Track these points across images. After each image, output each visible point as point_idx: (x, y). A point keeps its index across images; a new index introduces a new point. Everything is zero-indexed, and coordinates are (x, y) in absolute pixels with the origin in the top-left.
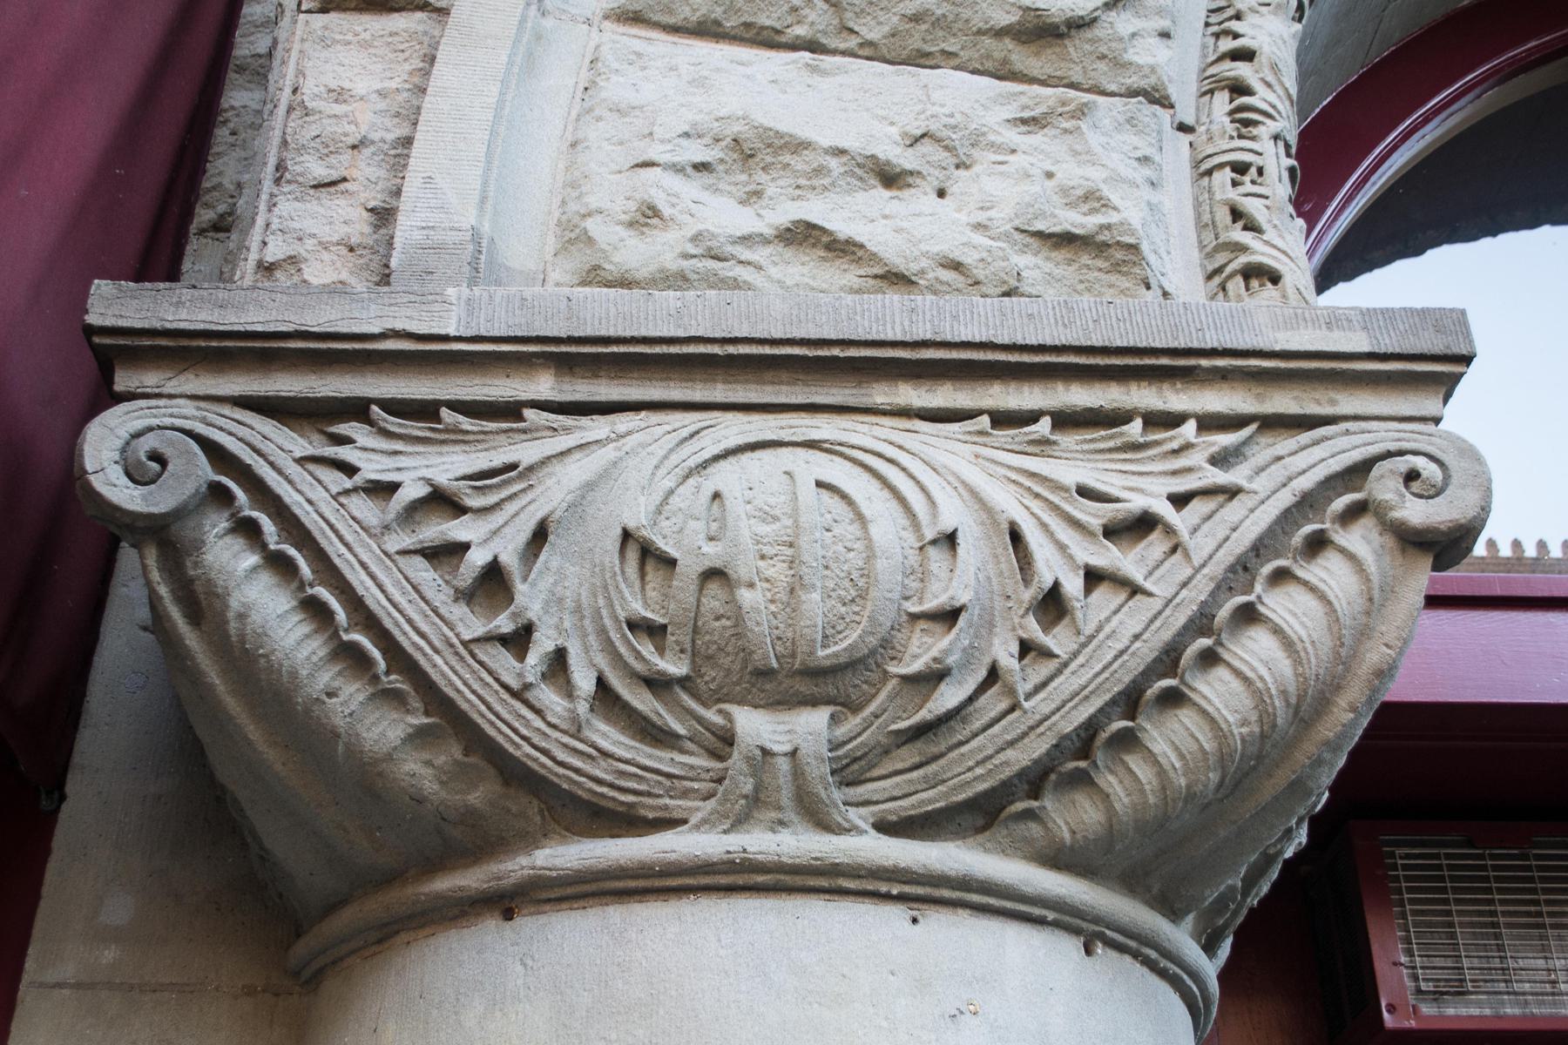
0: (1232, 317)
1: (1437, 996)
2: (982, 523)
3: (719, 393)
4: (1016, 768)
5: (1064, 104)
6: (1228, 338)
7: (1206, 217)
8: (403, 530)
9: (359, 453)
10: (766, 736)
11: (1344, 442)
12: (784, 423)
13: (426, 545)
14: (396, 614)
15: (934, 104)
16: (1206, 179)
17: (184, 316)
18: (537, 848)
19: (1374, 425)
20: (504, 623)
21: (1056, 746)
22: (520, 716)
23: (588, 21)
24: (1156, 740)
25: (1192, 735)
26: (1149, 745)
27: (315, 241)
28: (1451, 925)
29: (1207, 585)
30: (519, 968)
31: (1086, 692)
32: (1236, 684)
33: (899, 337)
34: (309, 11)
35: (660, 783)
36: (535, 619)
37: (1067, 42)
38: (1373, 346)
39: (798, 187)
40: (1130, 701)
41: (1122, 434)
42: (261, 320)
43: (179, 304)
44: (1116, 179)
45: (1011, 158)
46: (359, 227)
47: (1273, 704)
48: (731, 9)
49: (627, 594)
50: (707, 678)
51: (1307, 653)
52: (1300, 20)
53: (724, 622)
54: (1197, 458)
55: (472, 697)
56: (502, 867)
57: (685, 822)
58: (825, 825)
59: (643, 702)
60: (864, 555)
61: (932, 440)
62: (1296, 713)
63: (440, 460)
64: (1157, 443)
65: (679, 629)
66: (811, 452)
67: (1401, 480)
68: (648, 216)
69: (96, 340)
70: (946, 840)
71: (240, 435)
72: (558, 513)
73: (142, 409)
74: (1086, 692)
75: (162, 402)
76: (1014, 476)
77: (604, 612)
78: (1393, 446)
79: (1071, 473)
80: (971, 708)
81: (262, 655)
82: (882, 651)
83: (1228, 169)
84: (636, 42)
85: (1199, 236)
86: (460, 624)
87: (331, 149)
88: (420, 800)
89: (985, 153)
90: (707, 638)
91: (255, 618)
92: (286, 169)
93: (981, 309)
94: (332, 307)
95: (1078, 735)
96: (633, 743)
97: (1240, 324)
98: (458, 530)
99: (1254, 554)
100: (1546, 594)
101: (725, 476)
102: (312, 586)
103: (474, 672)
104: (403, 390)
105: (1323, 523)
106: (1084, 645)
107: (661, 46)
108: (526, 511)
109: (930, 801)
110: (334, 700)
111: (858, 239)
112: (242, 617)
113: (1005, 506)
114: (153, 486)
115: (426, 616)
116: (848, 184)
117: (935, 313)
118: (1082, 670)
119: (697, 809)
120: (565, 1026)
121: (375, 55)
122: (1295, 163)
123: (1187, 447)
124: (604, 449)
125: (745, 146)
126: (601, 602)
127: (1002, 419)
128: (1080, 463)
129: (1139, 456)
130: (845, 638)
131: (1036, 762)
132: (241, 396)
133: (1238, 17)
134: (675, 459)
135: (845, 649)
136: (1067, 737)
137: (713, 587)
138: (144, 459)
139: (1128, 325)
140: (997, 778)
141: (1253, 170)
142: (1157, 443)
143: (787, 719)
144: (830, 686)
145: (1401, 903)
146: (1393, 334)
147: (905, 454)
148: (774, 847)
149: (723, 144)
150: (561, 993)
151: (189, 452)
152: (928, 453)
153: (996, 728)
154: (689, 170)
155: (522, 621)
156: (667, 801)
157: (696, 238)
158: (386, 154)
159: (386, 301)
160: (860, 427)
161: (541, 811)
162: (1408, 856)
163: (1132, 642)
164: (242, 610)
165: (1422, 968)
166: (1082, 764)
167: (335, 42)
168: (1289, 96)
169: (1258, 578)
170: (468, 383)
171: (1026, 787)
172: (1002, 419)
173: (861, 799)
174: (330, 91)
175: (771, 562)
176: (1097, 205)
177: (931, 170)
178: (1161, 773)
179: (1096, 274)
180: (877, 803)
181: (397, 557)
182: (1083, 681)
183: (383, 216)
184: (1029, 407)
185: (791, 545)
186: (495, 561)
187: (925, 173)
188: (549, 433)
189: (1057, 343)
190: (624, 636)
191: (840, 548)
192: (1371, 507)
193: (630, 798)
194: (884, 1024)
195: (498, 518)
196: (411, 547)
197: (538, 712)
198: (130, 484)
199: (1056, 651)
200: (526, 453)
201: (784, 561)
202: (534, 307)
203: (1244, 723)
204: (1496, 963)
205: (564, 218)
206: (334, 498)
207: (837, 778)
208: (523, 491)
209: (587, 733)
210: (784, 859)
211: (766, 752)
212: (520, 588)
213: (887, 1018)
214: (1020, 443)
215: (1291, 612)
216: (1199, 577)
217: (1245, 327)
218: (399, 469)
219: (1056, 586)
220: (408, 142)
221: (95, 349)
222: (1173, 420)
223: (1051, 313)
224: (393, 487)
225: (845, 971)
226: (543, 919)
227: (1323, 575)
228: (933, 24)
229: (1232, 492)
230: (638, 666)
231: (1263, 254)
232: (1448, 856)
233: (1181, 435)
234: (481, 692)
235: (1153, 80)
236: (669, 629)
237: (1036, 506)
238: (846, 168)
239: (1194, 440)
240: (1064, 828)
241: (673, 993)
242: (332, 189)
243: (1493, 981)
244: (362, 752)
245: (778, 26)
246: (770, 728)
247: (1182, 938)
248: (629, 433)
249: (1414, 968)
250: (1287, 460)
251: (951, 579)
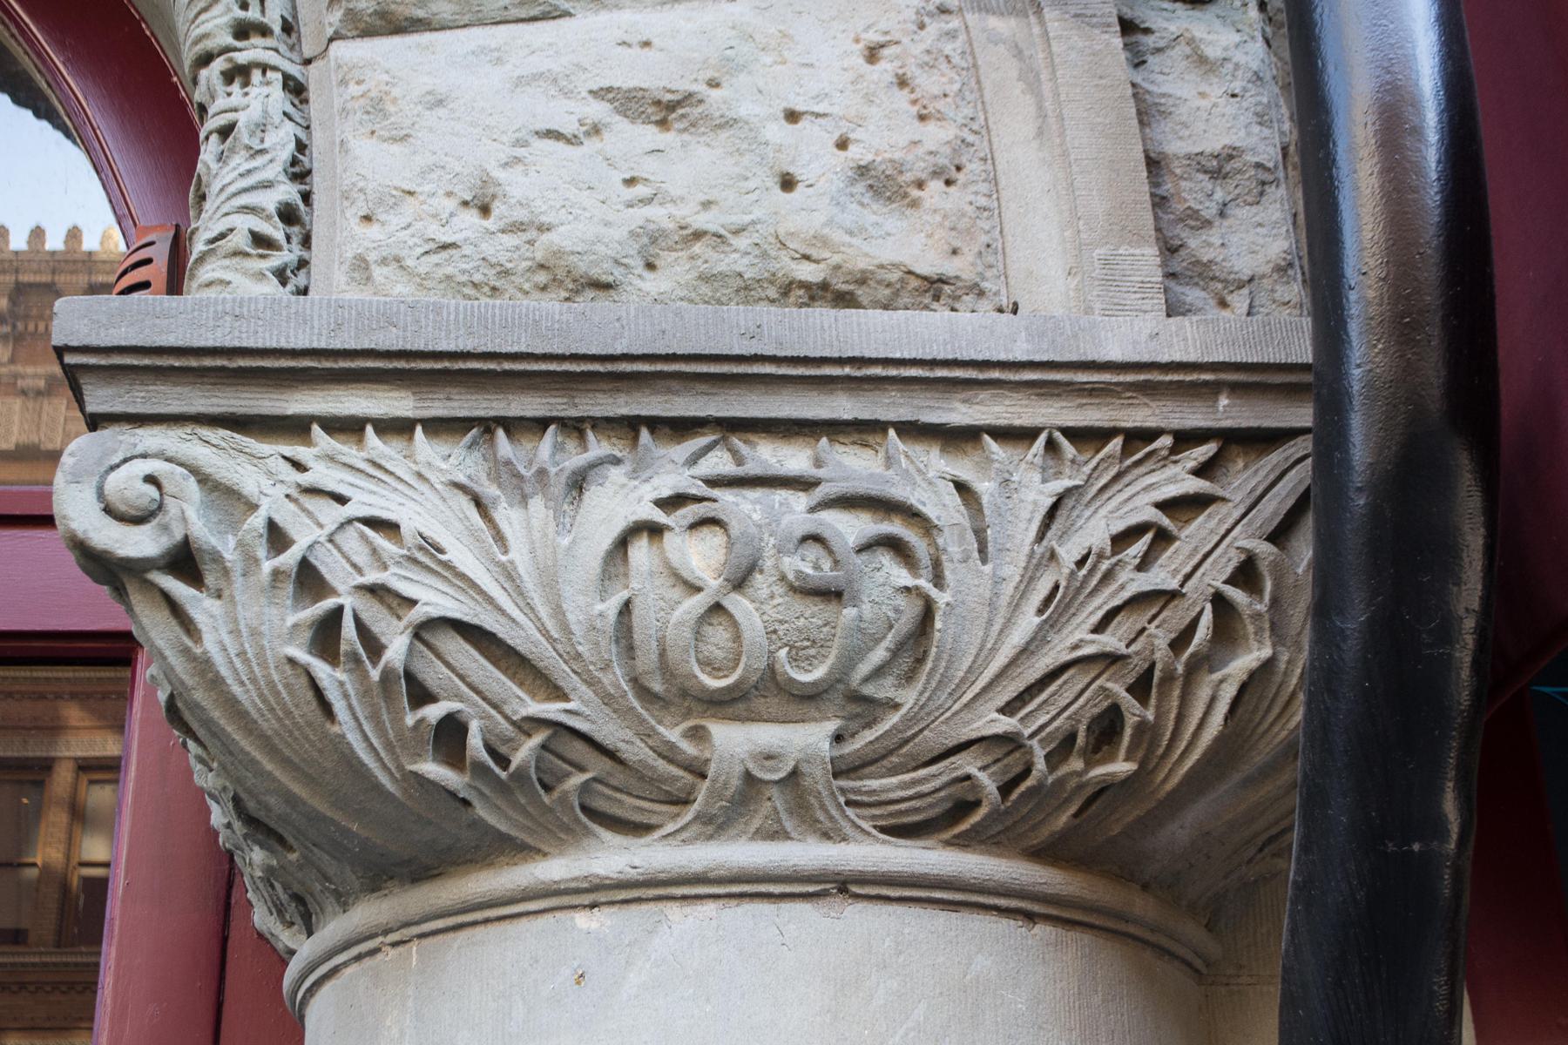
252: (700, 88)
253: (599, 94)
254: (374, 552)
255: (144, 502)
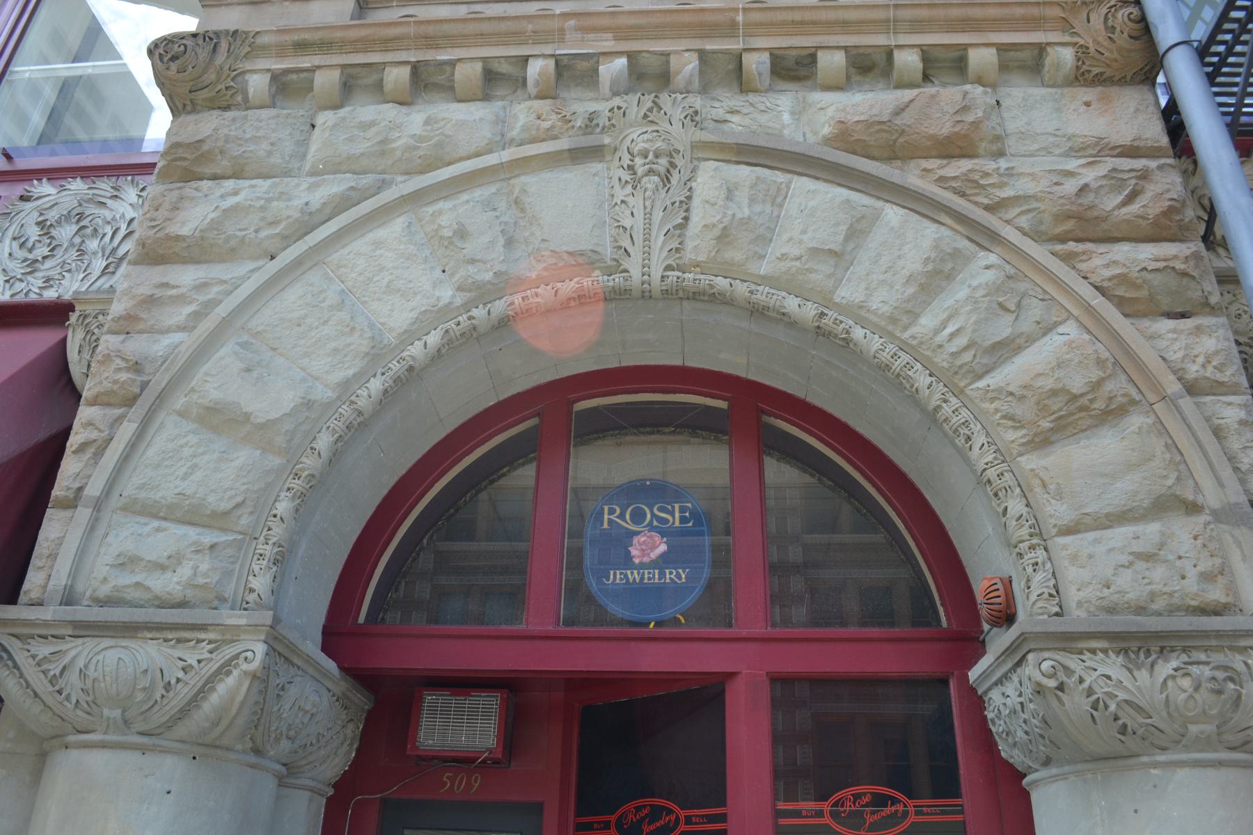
127: (166, 640)
200: (63, 647)
252: (1157, 551)
253: (1131, 554)
254: (1106, 683)
255: (1051, 673)
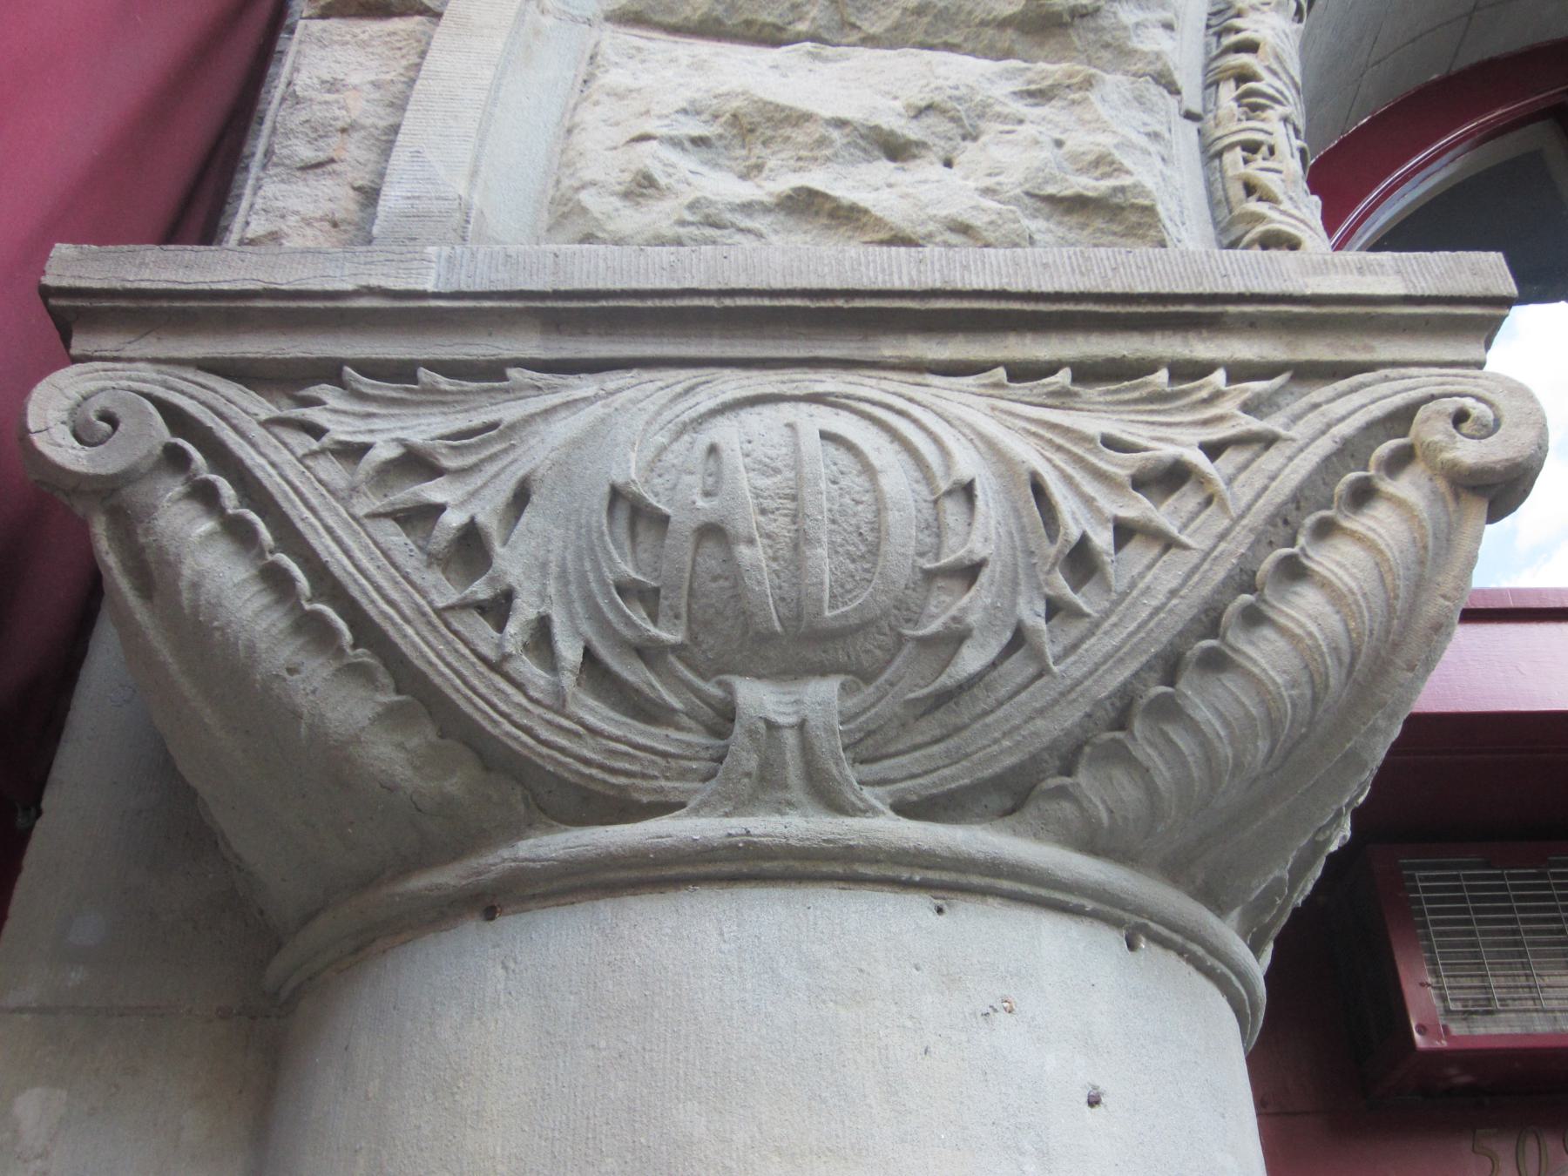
0: (1258, 263)
1: (1467, 1015)
2: (1001, 476)
3: (715, 349)
4: (1046, 740)
5: (1070, 77)
6: (1255, 282)
7: (1220, 194)
8: (373, 494)
9: (329, 416)
10: (770, 707)
11: (1384, 388)
12: (786, 378)
13: (397, 507)
14: (364, 581)
15: (937, 78)
16: (1216, 162)
17: (146, 276)
18: (521, 839)
19: (1414, 371)
20: (481, 590)
21: (1089, 716)
22: (499, 690)
23: (589, 22)
24: (1198, 707)
25: (1237, 700)
26: (1190, 712)
27: (297, 218)
28: (1474, 944)
29: (1246, 537)
30: (500, 972)
31: (1121, 654)
32: (1281, 644)
33: (907, 286)
34: (310, 18)
35: (654, 762)
36: (515, 584)
37: (1071, 31)
38: (1407, 287)
39: (799, 159)
40: (1170, 666)
41: (1146, 384)
42: (228, 278)
43: (143, 264)
44: (1125, 145)
45: (1019, 128)
46: (345, 203)
47: (1324, 662)
48: (733, 8)
49: (615, 555)
50: (704, 646)
51: (1359, 606)
52: (1300, 21)
53: (722, 583)
54: (1228, 406)
55: (447, 671)
56: (482, 861)
57: (682, 805)
58: (835, 804)
59: (634, 673)
60: (874, 508)
61: (945, 394)
62: (1350, 673)
63: (415, 422)
64: (1185, 393)
65: (673, 591)
66: (814, 406)
67: (1450, 421)
68: (643, 187)
69: (53, 302)
70: (972, 823)
71: (203, 398)
72: (541, 471)
73: (97, 371)
74: (1121, 654)
75: (118, 365)
76: (1033, 428)
77: (591, 576)
78: (1435, 390)
79: (1094, 424)
80: (995, 674)
81: (217, 628)
82: (896, 612)
83: (1238, 150)
84: (634, 38)
85: (1212, 215)
86: (433, 591)
87: (321, 133)
88: (392, 789)
89: (992, 124)
90: (704, 601)
91: (209, 586)
92: (273, 153)
93: (993, 258)
94: (304, 266)
95: (1112, 704)
96: (624, 719)
97: (1267, 269)
98: (433, 491)
99: (1294, 506)
100: (1558, 605)
101: (725, 432)
102: (271, 552)
103: (448, 643)
104: (378, 350)
105: (1365, 468)
106: (1116, 603)
107: (660, 45)
108: (508, 472)
109: (953, 778)
110: (296, 677)
111: (862, 204)
112: (195, 586)
113: (1025, 456)
114: (101, 447)
115: (397, 583)
116: (852, 155)
117: (944, 263)
118: (1115, 631)
119: (696, 791)
120: (548, 1033)
121: (372, 53)
122: (1305, 145)
123: (1216, 396)
124: (592, 407)
125: (745, 121)
126: (588, 565)
127: (1022, 372)
128: (1103, 415)
129: (1167, 406)
130: (855, 597)
131: (1068, 733)
132: (205, 359)
133: (1239, 15)
134: (667, 415)
135: (855, 609)
136: (1098, 704)
137: (710, 547)
138: (94, 418)
139: (1149, 271)
140: (1026, 750)
141: (1264, 149)
142: (1185, 393)
143: (793, 689)
144: (840, 652)
145: (1424, 925)
146: (1428, 278)
147: (915, 406)
148: (781, 829)
149: (723, 120)
150: (545, 997)
151: (144, 411)
152: (941, 404)
153: (1024, 696)
154: (687, 144)
155: (500, 588)
156: (663, 783)
157: (692, 206)
158: (377, 139)
159: (362, 259)
160: (867, 381)
161: (525, 799)
162: (1427, 879)
163: (1169, 600)
164: (196, 579)
165: (1450, 988)
166: (1119, 735)
167: (333, 42)
168: (1295, 84)
169: (1301, 530)
170: (447, 342)
171: (1057, 763)
172: (1022, 372)
173: (878, 777)
174: (323, 82)
175: (772, 516)
176: (1107, 169)
177: (937, 141)
178: (1204, 742)
179: (1111, 238)
180: (894, 781)
181: (365, 521)
182: (1116, 641)
183: (369, 196)
184: (1047, 358)
185: (794, 498)
186: (472, 520)
187: (930, 143)
188: (534, 392)
189: (1075, 290)
190: (612, 602)
191: (847, 500)
192: (1418, 452)
193: (622, 780)
194: (909, 1024)
195: (477, 480)
196: (381, 510)
197: (519, 686)
198: (76, 444)
199: (1086, 609)
200: (508, 412)
201: (786, 515)
202: (518, 263)
203: (1294, 684)
204: (1522, 981)
205: (559, 194)
206: (300, 461)
207: (851, 755)
208: (505, 451)
209: (572, 708)
210: (792, 842)
211: (771, 726)
212: (498, 549)
213: (911, 1017)
214: (1039, 395)
215: (1339, 564)
216: (1238, 529)
217: (1273, 273)
218: (371, 431)
219: (1084, 540)
220: (395, 129)
221: (53, 313)
222: (1202, 370)
223: (1067, 261)
224: (365, 448)
225: (864, 965)
226: (526, 917)
227: (1371, 523)
228: (935, 16)
229: (1268, 441)
230: (627, 633)
231: (1280, 222)
232: (1468, 878)
233: (1210, 384)
234: (456, 664)
235: (1159, 66)
236: (663, 592)
237: (1058, 459)
238: (849, 139)
239: (1224, 388)
240: (1101, 807)
241: (670, 993)
242: (319, 171)
243: (1520, 999)
244: (326, 734)
245: (779, 22)
246: (774, 698)
247: (1228, 934)
248: (620, 390)
249: (1441, 988)
250: (1324, 407)
251: (969, 534)
